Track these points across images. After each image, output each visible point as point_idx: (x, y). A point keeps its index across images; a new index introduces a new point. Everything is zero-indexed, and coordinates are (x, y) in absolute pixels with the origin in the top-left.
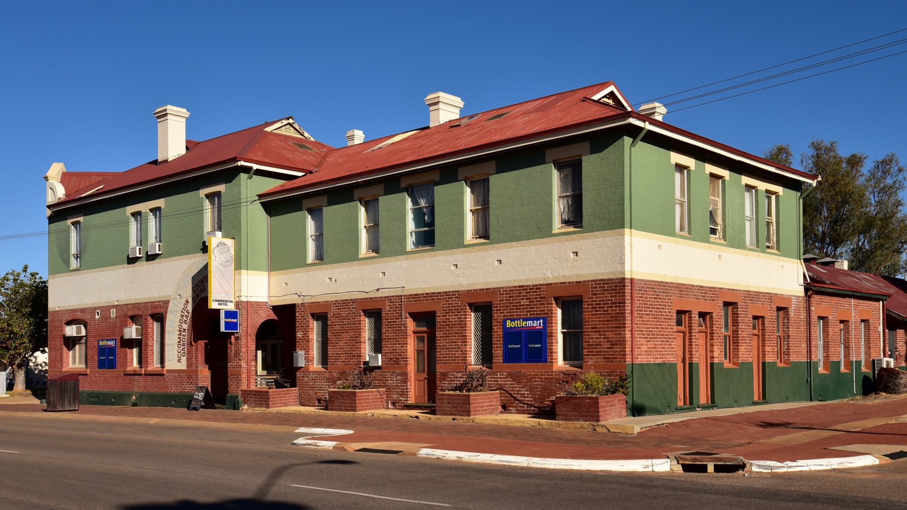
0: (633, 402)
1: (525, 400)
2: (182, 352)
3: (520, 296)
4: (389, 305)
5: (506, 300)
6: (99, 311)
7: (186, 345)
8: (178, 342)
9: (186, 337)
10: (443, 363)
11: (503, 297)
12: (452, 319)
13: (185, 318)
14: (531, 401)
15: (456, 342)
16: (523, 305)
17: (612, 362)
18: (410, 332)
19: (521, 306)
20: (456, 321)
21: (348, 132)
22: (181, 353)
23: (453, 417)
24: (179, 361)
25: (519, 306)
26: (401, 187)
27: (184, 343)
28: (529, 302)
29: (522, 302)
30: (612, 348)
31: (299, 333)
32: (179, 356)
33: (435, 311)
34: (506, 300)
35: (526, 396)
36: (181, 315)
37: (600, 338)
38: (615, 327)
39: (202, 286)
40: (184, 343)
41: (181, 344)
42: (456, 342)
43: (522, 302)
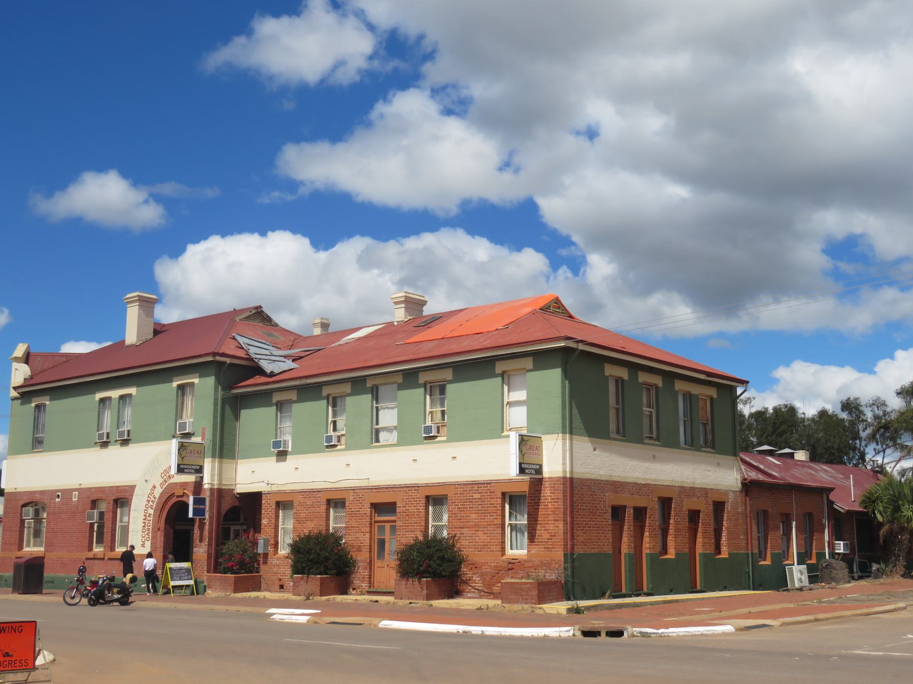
1: (476, 586)
2: (146, 536)
6: (60, 494)
7: (151, 529)
9: (151, 522)
11: (457, 491)
12: (411, 509)
13: (151, 503)
16: (475, 499)
27: (149, 527)
34: (460, 494)
36: (147, 500)
40: (149, 527)
41: (146, 528)
43: (475, 496)
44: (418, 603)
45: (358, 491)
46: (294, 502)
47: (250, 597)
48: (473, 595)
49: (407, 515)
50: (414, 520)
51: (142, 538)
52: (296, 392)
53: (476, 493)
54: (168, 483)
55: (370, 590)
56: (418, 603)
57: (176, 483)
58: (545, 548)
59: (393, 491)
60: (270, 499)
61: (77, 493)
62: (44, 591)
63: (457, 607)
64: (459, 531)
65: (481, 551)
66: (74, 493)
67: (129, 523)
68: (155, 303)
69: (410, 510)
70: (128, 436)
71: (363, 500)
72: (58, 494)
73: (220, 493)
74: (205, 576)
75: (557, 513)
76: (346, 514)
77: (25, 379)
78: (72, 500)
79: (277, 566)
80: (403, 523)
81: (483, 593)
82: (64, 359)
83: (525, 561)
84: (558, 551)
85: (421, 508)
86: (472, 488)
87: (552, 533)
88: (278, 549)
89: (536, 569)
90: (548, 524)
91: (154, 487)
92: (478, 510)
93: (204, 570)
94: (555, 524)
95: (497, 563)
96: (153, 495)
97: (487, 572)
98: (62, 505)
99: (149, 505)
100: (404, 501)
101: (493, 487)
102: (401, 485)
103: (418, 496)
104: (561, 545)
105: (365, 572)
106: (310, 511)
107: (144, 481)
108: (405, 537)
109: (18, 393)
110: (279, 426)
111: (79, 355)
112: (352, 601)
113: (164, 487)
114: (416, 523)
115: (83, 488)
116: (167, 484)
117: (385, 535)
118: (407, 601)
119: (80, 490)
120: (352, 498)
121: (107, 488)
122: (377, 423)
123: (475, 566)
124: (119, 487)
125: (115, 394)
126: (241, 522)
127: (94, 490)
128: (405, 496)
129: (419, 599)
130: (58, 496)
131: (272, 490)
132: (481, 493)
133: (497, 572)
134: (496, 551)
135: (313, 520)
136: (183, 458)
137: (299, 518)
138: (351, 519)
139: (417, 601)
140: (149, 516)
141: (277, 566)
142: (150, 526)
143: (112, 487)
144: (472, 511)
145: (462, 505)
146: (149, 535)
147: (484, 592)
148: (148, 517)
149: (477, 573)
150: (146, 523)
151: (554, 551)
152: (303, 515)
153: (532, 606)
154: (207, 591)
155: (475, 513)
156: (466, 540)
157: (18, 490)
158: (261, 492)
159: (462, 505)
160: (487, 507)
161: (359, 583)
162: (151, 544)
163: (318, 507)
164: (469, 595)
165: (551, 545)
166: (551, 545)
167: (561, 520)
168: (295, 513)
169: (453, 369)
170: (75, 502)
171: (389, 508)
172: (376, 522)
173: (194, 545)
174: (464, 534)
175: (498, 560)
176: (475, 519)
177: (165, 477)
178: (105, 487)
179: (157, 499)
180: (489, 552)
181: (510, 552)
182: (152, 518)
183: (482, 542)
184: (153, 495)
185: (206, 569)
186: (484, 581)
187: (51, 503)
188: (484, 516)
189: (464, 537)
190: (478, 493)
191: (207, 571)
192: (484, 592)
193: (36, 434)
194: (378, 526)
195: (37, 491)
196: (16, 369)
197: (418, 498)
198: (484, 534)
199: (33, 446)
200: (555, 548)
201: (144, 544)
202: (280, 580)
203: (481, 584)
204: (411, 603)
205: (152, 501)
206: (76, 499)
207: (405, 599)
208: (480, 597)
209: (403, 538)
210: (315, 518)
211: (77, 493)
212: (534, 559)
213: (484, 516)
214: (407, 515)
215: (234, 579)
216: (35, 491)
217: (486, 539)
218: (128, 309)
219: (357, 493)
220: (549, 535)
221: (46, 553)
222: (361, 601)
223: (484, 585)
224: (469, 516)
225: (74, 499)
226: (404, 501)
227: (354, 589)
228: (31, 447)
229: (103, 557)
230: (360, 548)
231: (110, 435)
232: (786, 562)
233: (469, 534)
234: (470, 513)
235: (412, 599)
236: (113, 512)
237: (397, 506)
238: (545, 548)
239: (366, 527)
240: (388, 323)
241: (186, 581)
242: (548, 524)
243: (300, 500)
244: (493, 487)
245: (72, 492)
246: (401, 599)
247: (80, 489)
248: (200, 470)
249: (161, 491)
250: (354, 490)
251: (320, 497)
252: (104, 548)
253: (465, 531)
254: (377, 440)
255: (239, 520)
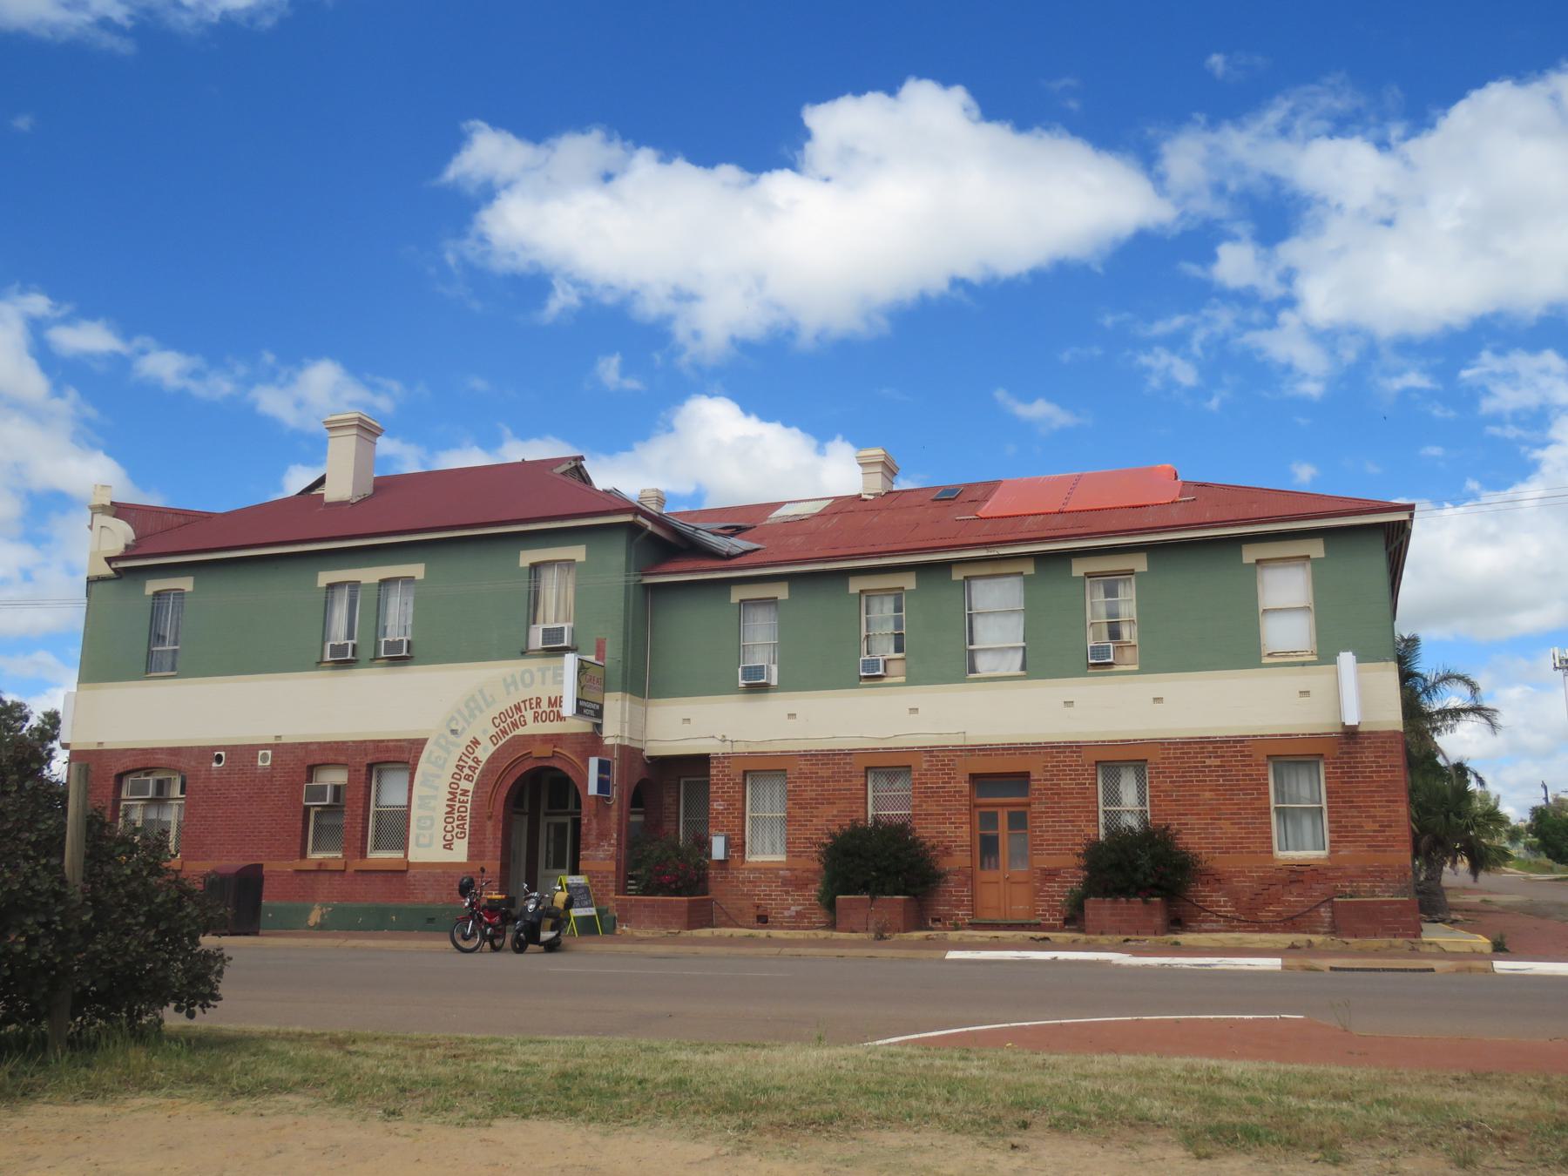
0: (987, 908)
1: (1220, 911)
2: (456, 830)
3: (1203, 753)
4: (928, 761)
5: (1175, 758)
6: (223, 754)
7: (468, 818)
8: (447, 813)
9: (468, 805)
10: (1048, 854)
11: (1168, 754)
12: (1065, 784)
13: (466, 771)
14: (1234, 912)
15: (1073, 821)
16: (1210, 766)
17: (1385, 851)
18: (1272, 809)
19: (1206, 767)
20: (1073, 789)
21: (1447, 505)
22: (454, 833)
23: (1126, 937)
24: (448, 846)
25: (1203, 767)
26: (1073, 575)
27: (463, 814)
28: (1221, 761)
29: (1208, 762)
30: (1384, 831)
31: (715, 803)
32: (449, 837)
33: (1029, 772)
34: (1175, 758)
35: (1222, 903)
36: (457, 766)
37: (1361, 817)
38: (1387, 801)
39: (516, 717)
40: (463, 814)
41: (455, 816)
42: (1073, 821)
43: (1208, 762)
44: (1145, 940)
45: (940, 754)
46: (788, 772)
47: (731, 936)
48: (1215, 926)
49: (1056, 794)
50: (1073, 803)
51: (444, 833)
52: (1033, 563)
53: (1210, 757)
54: (511, 735)
55: (973, 921)
56: (1145, 940)
57: (534, 736)
58: (1369, 846)
59: (1020, 754)
60: (729, 767)
61: (269, 752)
62: (261, 932)
63: (1238, 946)
64: (1175, 820)
65: (1229, 853)
66: (261, 752)
67: (409, 806)
68: (379, 435)
69: (1062, 786)
70: (353, 654)
71: (953, 769)
72: (216, 753)
73: (630, 754)
74: (612, 900)
75: (1393, 789)
76: (914, 793)
77: (127, 546)
78: (257, 765)
79: (750, 882)
80: (1046, 808)
81: (1235, 923)
82: (182, 520)
83: (1326, 868)
84: (1400, 851)
85: (1087, 782)
86: (1203, 748)
87: (1382, 821)
88: (745, 853)
89: (1352, 881)
90: (1375, 807)
91: (476, 742)
92: (1217, 785)
93: (609, 891)
94: (1389, 807)
95: (1263, 872)
96: (472, 757)
97: (1243, 887)
98: (229, 774)
99: (463, 775)
100: (1048, 771)
101: (1249, 746)
102: (1041, 743)
103: (1080, 763)
104: (1405, 841)
105: (963, 891)
106: (826, 788)
107: (449, 732)
108: (1052, 831)
109: (114, 570)
110: (742, 644)
111: (206, 515)
112: (988, 940)
113: (500, 743)
114: (1078, 807)
115: (283, 744)
116: (507, 737)
117: (997, 828)
118: (1119, 937)
119: (278, 749)
120: (925, 766)
121: (351, 744)
122: (971, 643)
123: (1216, 879)
124: (383, 741)
125: (369, 575)
126: (569, 810)
127: (315, 747)
128: (1049, 762)
129: (1144, 934)
130: (219, 759)
131: (734, 751)
132: (1223, 756)
133: (1266, 887)
134: (1260, 852)
135: (834, 803)
136: (582, 689)
137: (801, 799)
138: (925, 802)
139: (1144, 937)
140: (461, 795)
141: (750, 882)
142: (466, 812)
143: (365, 741)
144: (1203, 786)
145: (1180, 777)
146: (463, 828)
147: (1239, 920)
148: (458, 797)
149: (1221, 889)
150: (456, 808)
151: (1234, 853)
152: (810, 794)
153: (1344, 940)
154: (618, 927)
155: (1210, 791)
156: (1191, 834)
157: (106, 747)
158: (709, 754)
159: (1180, 777)
160: (1237, 780)
161: (948, 910)
162: (469, 843)
163: (846, 781)
164: (1205, 926)
165: (1383, 841)
166: (1383, 841)
167: (1402, 801)
168: (789, 791)
169: (1147, 555)
170: (264, 768)
171: (1019, 781)
172: (975, 806)
173: (582, 846)
174: (1187, 824)
175: (1266, 867)
176: (1210, 800)
177: (502, 725)
178: (344, 743)
179: (482, 764)
180: (1245, 855)
181: (1286, 855)
182: (470, 798)
183: (1227, 838)
184: (472, 757)
185: (614, 888)
186: (1237, 903)
187: (200, 771)
188: (1231, 795)
189: (1188, 829)
190: (1215, 757)
191: (616, 890)
192: (1239, 920)
193: (154, 647)
194: (982, 814)
195: (162, 749)
196: (102, 527)
197: (1080, 766)
198: (1232, 824)
199: (147, 667)
200: (1393, 846)
201: (450, 844)
202: (758, 907)
203: (1231, 907)
204: (1127, 940)
205: (470, 767)
206: (269, 763)
207: (1110, 933)
208: (1232, 930)
209: (1048, 831)
210: (841, 799)
211: (269, 752)
212: (1347, 865)
213: (1231, 795)
214: (1056, 794)
215: (687, 904)
216: (153, 749)
217: (1237, 833)
218: (330, 440)
219: (938, 756)
220: (1378, 825)
221: (186, 863)
222: (1008, 938)
223: (1237, 909)
224: (1198, 795)
225: (260, 763)
226: (1048, 771)
227: (934, 920)
228: (144, 668)
229: (343, 868)
230: (949, 851)
231: (359, 650)
232: (1080, 889)
233: (1200, 824)
234: (1199, 791)
235: (1130, 934)
236: (366, 786)
237: (1032, 778)
238: (1369, 846)
239: (963, 814)
240: (836, 498)
241: (587, 909)
242: (1375, 807)
243: (801, 769)
244: (1249, 746)
245: (258, 750)
246: (1102, 933)
247: (277, 745)
248: (599, 713)
249: (492, 749)
250: (930, 752)
251: (850, 764)
252: (344, 851)
253: (1190, 819)
254: (973, 669)
255: (566, 807)
